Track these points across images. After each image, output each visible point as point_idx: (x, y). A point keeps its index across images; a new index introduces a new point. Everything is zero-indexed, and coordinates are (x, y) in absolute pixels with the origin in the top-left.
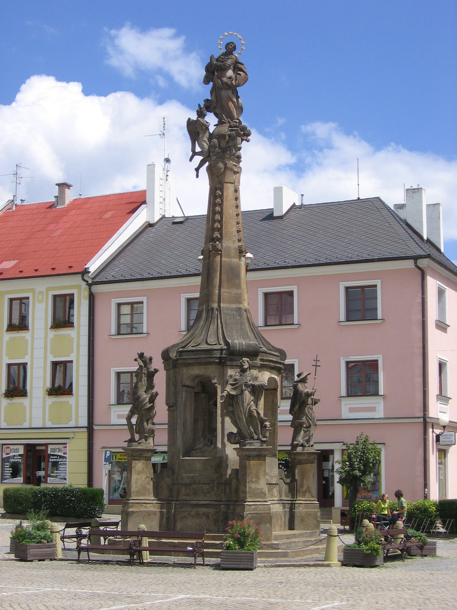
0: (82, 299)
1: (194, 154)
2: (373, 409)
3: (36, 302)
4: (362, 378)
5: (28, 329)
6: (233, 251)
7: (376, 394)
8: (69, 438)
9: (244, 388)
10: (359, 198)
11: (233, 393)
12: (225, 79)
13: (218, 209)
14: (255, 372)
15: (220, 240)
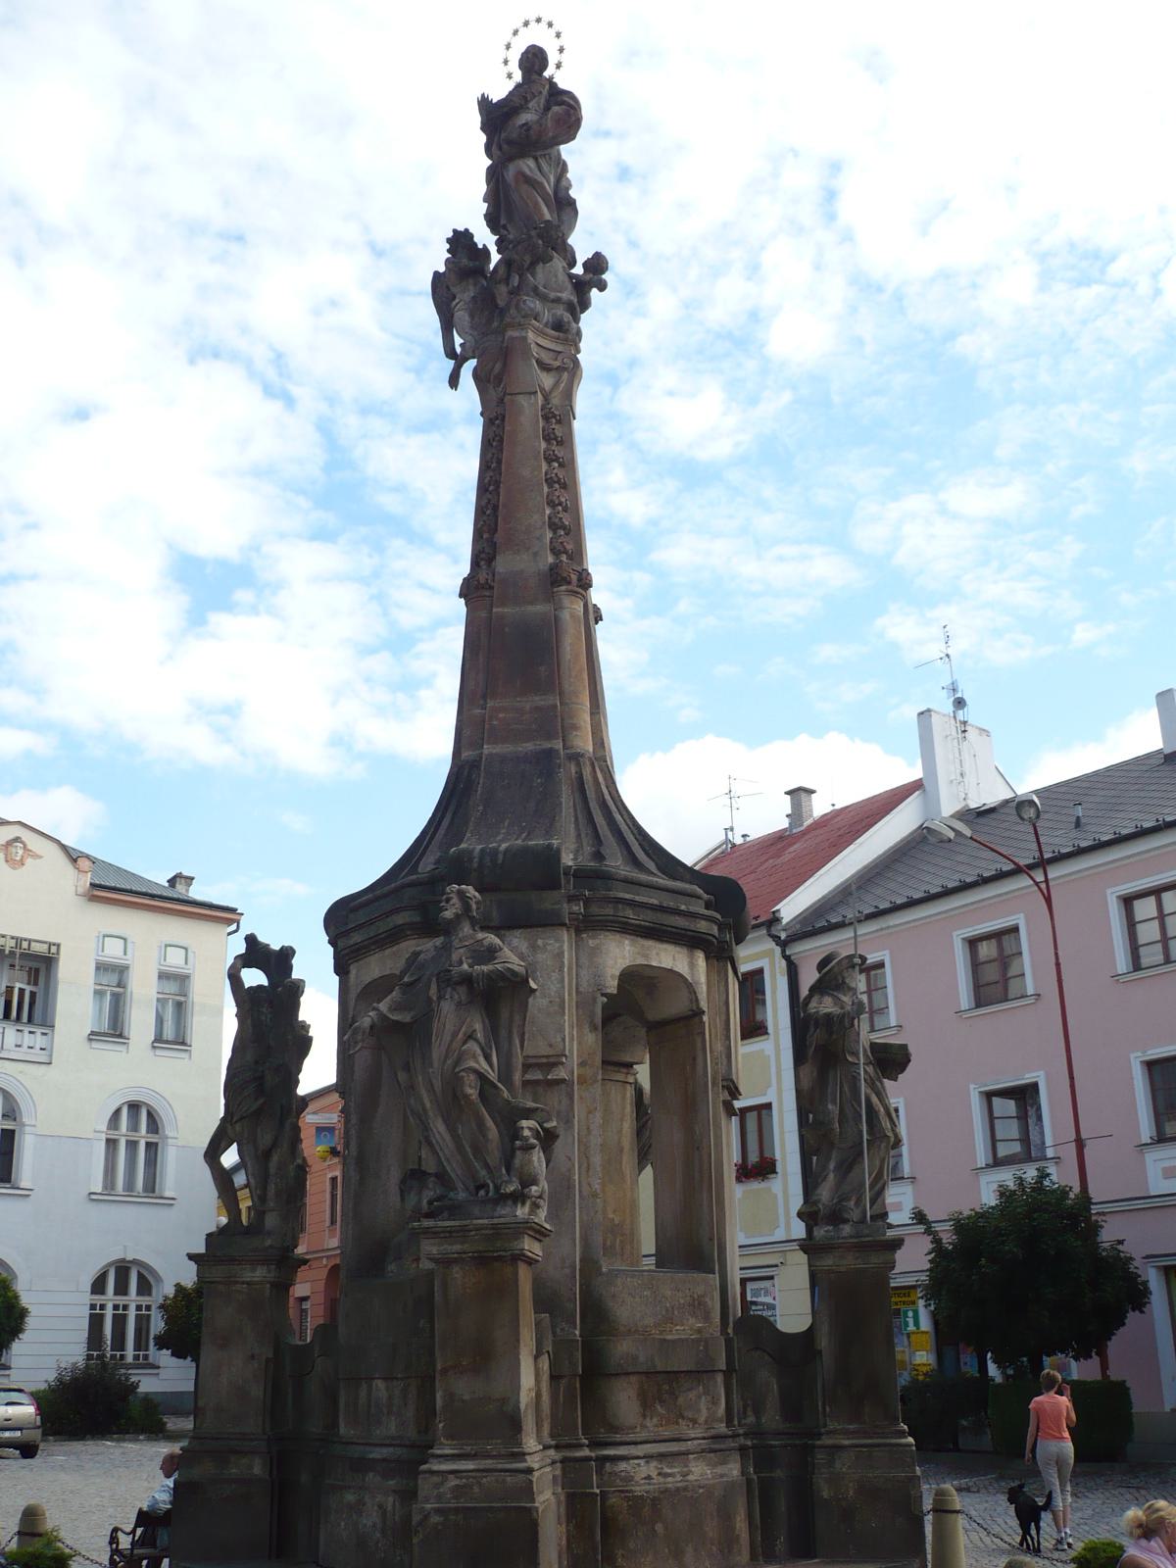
0: (778, 975)
8: (776, 1266)
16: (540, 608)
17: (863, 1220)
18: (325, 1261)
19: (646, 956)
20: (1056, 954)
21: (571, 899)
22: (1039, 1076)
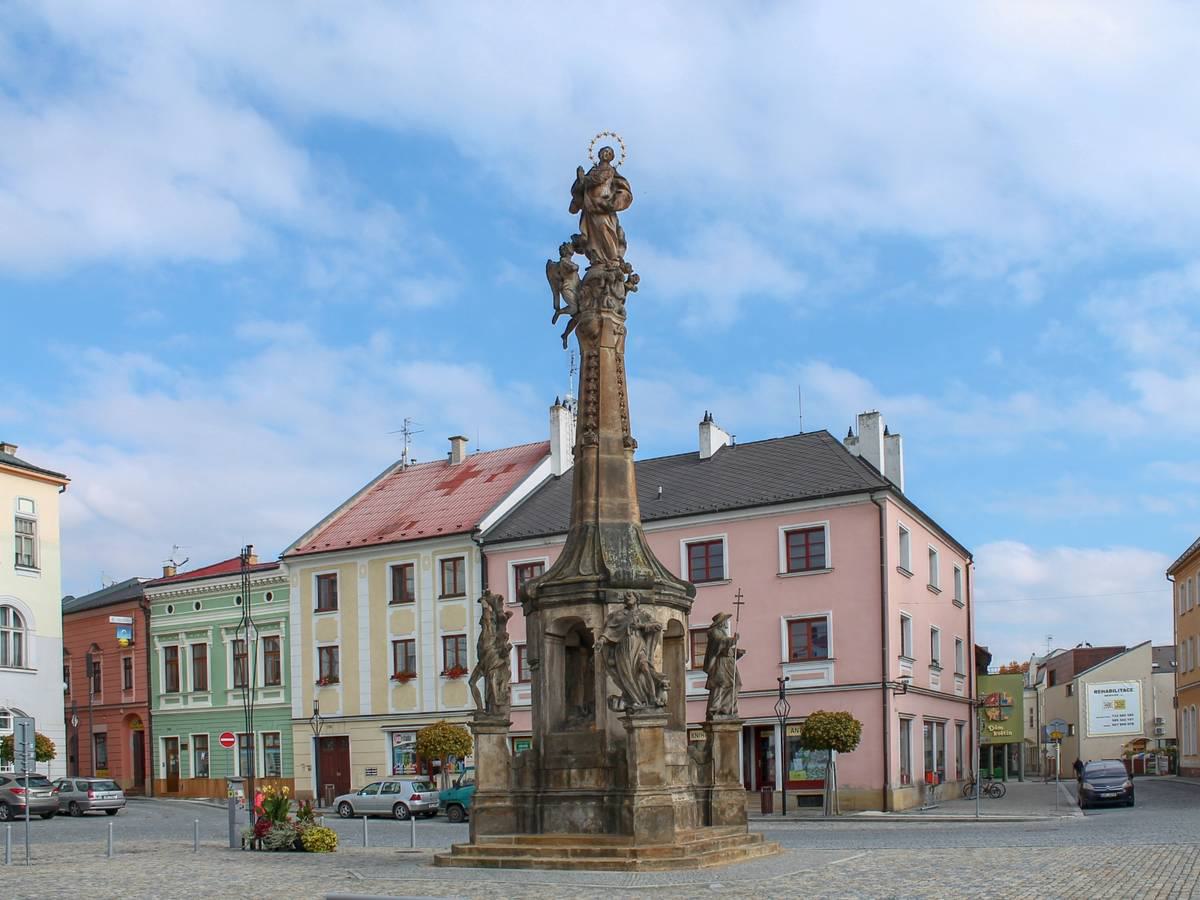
0: (474, 563)
2: (821, 676)
3: (422, 571)
4: (810, 639)
5: (413, 600)
6: (616, 444)
7: (825, 658)
9: (629, 633)
11: (615, 640)
12: (598, 200)
13: (592, 385)
14: (647, 610)
15: (596, 429)
16: (620, 457)
18: (122, 711)
21: (656, 593)
22: (314, 574)
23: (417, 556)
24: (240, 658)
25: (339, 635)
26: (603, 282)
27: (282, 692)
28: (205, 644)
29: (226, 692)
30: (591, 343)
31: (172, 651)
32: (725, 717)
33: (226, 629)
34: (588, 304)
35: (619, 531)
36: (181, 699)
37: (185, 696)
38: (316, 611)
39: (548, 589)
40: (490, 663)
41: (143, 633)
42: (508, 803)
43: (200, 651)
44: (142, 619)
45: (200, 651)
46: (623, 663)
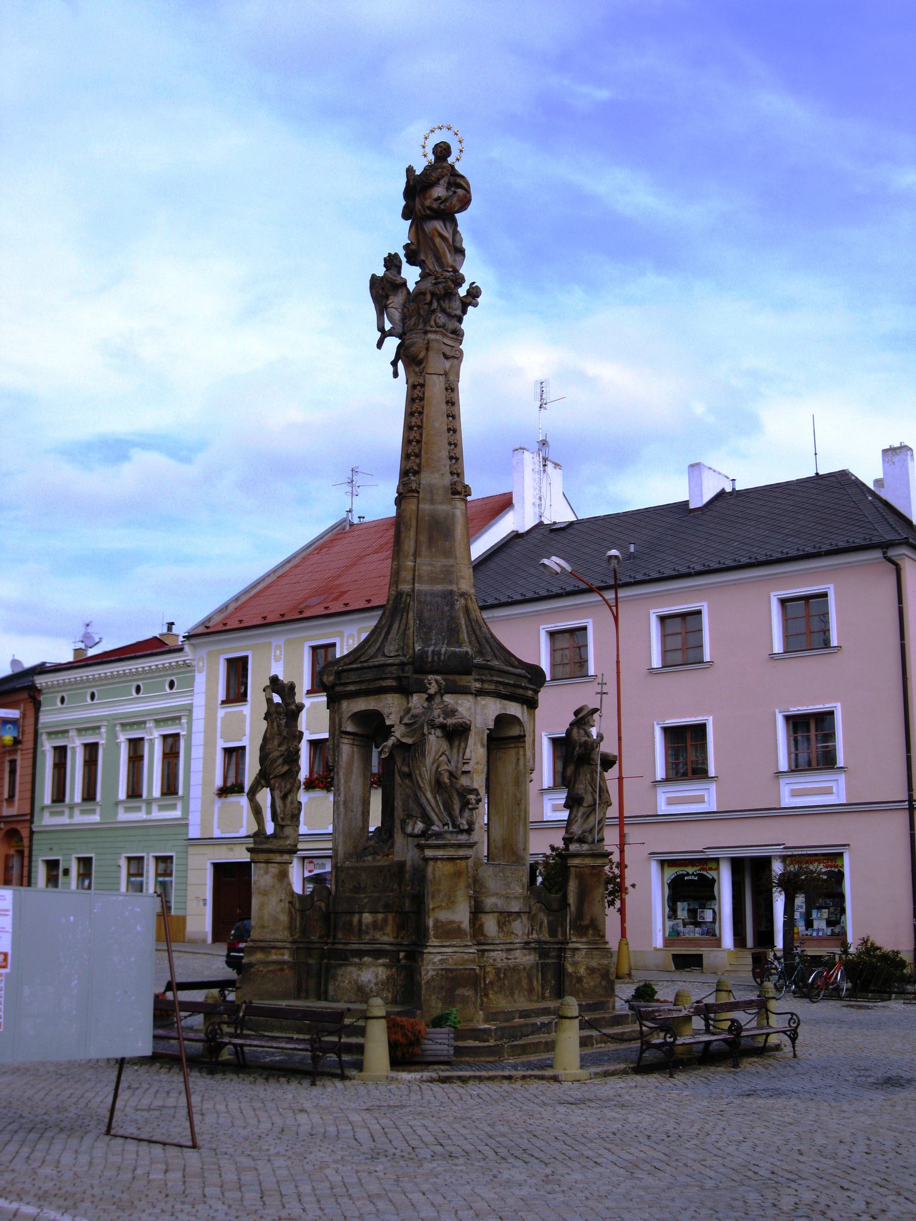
1: (384, 334)
4: (812, 736)
9: (426, 731)
10: (817, 474)
11: (409, 741)
17: (593, 842)
19: (505, 709)
20: (618, 655)
21: (476, 680)
23: (340, 634)
24: (136, 759)
25: (247, 732)
26: (428, 297)
27: (179, 805)
28: (142, 739)
29: (117, 803)
30: (417, 369)
31: (61, 752)
32: (585, 847)
33: (123, 725)
34: (412, 323)
35: (439, 599)
36: (67, 811)
37: (149, 802)
38: (223, 702)
39: (345, 674)
40: (277, 767)
41: (30, 729)
42: (286, 957)
43: (91, 749)
44: (31, 713)
45: (91, 749)
46: (417, 772)
